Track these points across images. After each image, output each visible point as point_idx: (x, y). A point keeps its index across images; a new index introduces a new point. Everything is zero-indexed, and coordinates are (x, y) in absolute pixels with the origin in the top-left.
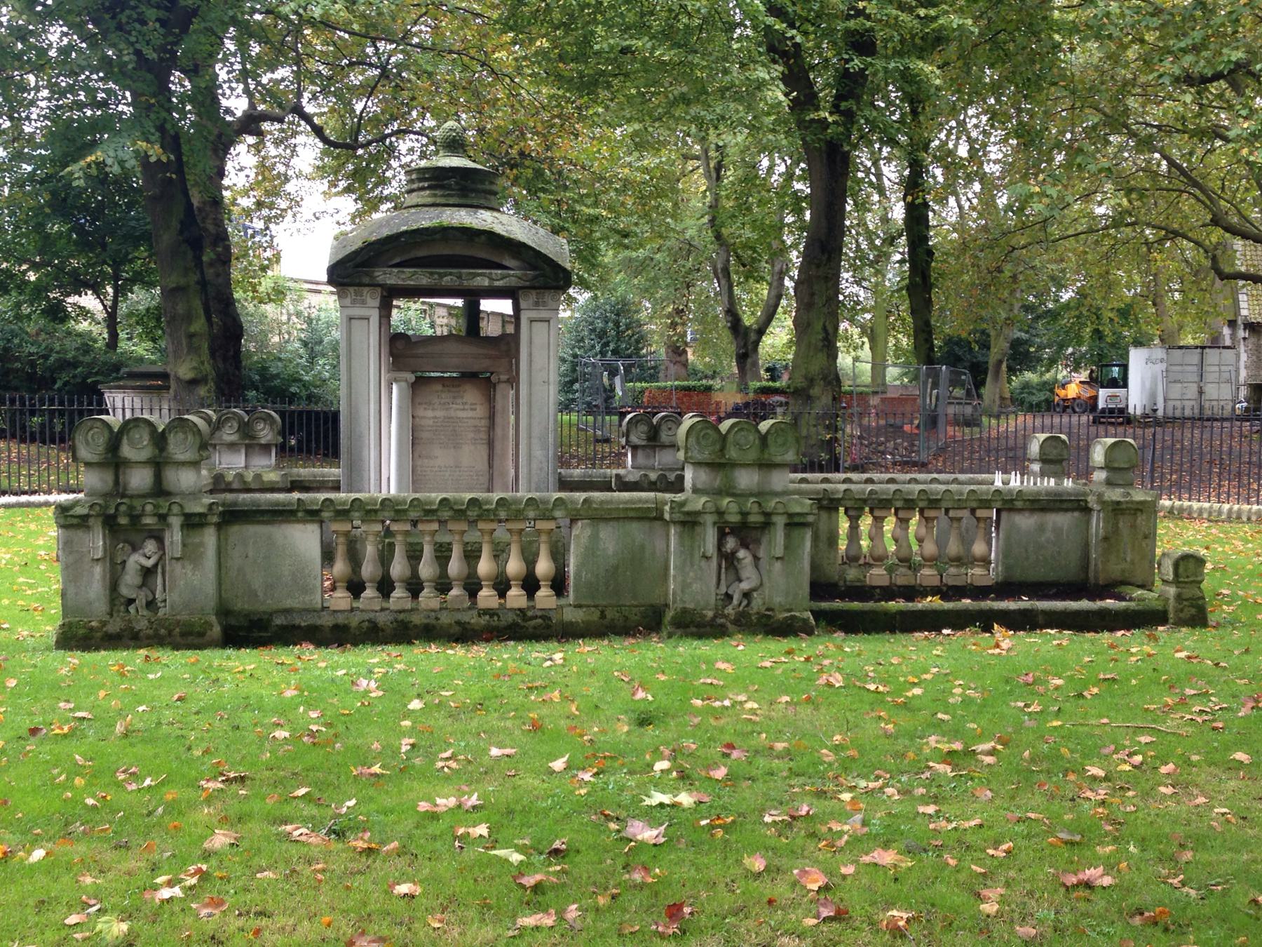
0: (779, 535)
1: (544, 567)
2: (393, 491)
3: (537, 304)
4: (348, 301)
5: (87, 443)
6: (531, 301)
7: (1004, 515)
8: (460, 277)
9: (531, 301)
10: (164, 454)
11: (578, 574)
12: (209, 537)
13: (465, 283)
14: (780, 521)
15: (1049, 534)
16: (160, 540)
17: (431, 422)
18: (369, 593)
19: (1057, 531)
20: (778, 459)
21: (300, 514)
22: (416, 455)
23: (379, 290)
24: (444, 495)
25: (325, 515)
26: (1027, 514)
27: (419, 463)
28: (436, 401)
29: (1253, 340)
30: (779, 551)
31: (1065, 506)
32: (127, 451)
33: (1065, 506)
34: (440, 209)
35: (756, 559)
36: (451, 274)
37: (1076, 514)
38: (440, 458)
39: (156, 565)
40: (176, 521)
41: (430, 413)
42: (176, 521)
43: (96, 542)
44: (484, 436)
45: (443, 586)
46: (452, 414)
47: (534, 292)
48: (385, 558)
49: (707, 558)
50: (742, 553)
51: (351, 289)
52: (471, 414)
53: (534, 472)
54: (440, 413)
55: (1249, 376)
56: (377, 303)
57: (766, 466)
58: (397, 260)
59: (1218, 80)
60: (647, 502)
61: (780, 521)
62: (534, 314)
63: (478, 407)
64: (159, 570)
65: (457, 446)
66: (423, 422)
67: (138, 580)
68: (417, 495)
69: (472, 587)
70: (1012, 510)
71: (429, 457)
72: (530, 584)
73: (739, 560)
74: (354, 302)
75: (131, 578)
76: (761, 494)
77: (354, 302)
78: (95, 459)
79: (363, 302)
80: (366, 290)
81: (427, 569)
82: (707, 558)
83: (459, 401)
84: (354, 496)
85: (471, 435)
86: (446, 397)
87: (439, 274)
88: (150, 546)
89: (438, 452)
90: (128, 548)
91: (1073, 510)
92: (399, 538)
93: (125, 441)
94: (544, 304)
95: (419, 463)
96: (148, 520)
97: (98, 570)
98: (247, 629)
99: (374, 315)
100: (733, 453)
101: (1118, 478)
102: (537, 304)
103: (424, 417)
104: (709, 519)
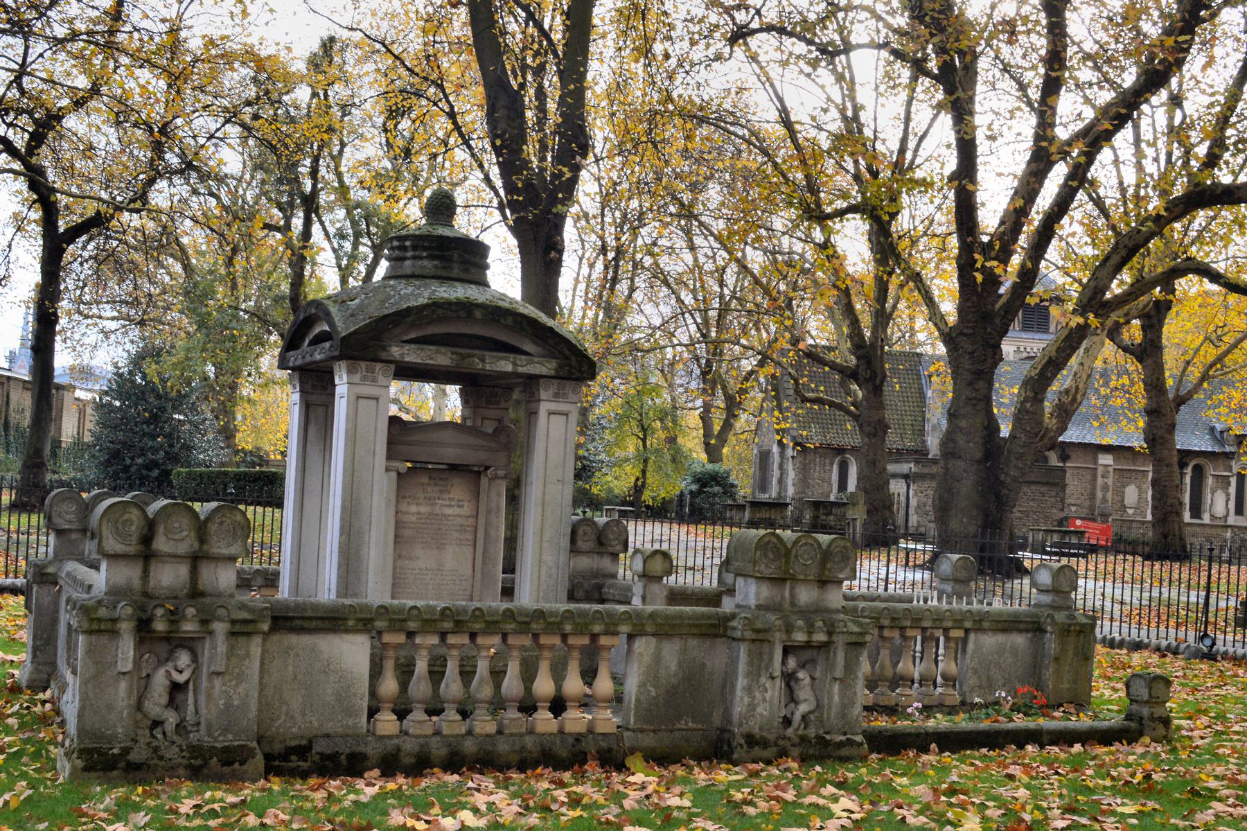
2: (286, 595)
3: (556, 395)
4: (357, 378)
6: (551, 392)
7: (972, 636)
9: (551, 392)
10: (205, 548)
12: (255, 647)
13: (488, 367)
17: (414, 519)
18: (418, 715)
21: (351, 623)
25: (380, 624)
27: (399, 564)
29: (799, 459)
30: (839, 672)
31: (1022, 626)
32: (161, 544)
33: (1022, 626)
38: (423, 559)
39: (187, 682)
40: (220, 628)
41: (413, 509)
42: (220, 628)
44: (470, 536)
45: (498, 704)
46: (437, 510)
47: (555, 381)
48: (436, 674)
49: (773, 678)
50: (801, 675)
51: (363, 364)
52: (457, 511)
53: (543, 578)
54: (423, 509)
55: (796, 493)
58: (412, 335)
59: (856, 213)
60: (709, 618)
62: (553, 406)
63: (466, 504)
64: (191, 686)
65: (441, 547)
66: (406, 518)
67: (164, 700)
70: (980, 630)
71: (410, 558)
73: (797, 680)
74: (364, 378)
77: (364, 378)
79: (374, 380)
80: (379, 366)
81: (420, 687)
82: (773, 678)
83: (447, 496)
85: (456, 535)
86: (432, 491)
88: (184, 659)
89: (419, 551)
94: (565, 396)
97: (123, 685)
102: (556, 395)
103: (408, 513)
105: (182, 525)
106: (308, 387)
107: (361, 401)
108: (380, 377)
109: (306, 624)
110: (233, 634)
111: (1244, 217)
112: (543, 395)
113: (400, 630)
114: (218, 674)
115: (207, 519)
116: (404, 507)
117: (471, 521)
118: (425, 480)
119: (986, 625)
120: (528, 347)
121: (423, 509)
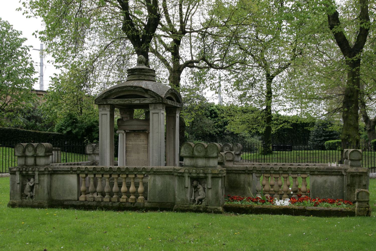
0: (210, 181)
1: (141, 189)
5: (18, 151)
6: (152, 107)
8: (131, 101)
9: (152, 107)
11: (150, 190)
14: (210, 176)
15: (328, 184)
16: (34, 178)
17: (131, 146)
19: (332, 183)
20: (211, 155)
22: (127, 155)
23: (109, 106)
24: (143, 167)
26: (320, 176)
28: (132, 139)
34: (141, 81)
35: (204, 188)
36: (128, 100)
37: (339, 177)
40: (37, 173)
41: (131, 143)
43: (18, 178)
44: (146, 150)
47: (153, 105)
54: (133, 143)
56: (109, 110)
57: (207, 157)
58: (115, 97)
61: (210, 176)
62: (154, 111)
63: (145, 141)
66: (129, 146)
67: (29, 190)
68: (127, 167)
69: (119, 194)
72: (119, 194)
74: (103, 110)
75: (27, 188)
76: (205, 167)
77: (103, 110)
78: (20, 155)
79: (105, 110)
83: (139, 139)
84: (101, 166)
87: (125, 100)
90: (27, 180)
91: (337, 175)
92: (115, 180)
93: (27, 150)
94: (157, 108)
95: (128, 158)
96: (30, 173)
98: (55, 203)
99: (108, 113)
100: (196, 154)
101: (355, 163)
102: (154, 108)
104: (186, 175)
105: (30, 148)
106: (122, 113)
107: (154, 114)
108: (107, 109)
109: (166, 173)
110: (39, 174)
111: (218, 9)
112: (150, 108)
113: (125, 174)
114: (210, 189)
115: (36, 147)
116: (128, 143)
117: (146, 146)
118: (133, 135)
119: (316, 173)
120: (146, 96)
121: (133, 143)
